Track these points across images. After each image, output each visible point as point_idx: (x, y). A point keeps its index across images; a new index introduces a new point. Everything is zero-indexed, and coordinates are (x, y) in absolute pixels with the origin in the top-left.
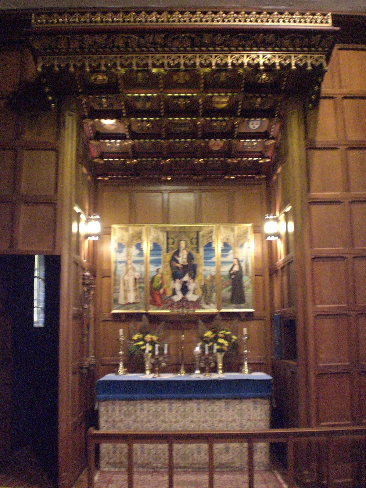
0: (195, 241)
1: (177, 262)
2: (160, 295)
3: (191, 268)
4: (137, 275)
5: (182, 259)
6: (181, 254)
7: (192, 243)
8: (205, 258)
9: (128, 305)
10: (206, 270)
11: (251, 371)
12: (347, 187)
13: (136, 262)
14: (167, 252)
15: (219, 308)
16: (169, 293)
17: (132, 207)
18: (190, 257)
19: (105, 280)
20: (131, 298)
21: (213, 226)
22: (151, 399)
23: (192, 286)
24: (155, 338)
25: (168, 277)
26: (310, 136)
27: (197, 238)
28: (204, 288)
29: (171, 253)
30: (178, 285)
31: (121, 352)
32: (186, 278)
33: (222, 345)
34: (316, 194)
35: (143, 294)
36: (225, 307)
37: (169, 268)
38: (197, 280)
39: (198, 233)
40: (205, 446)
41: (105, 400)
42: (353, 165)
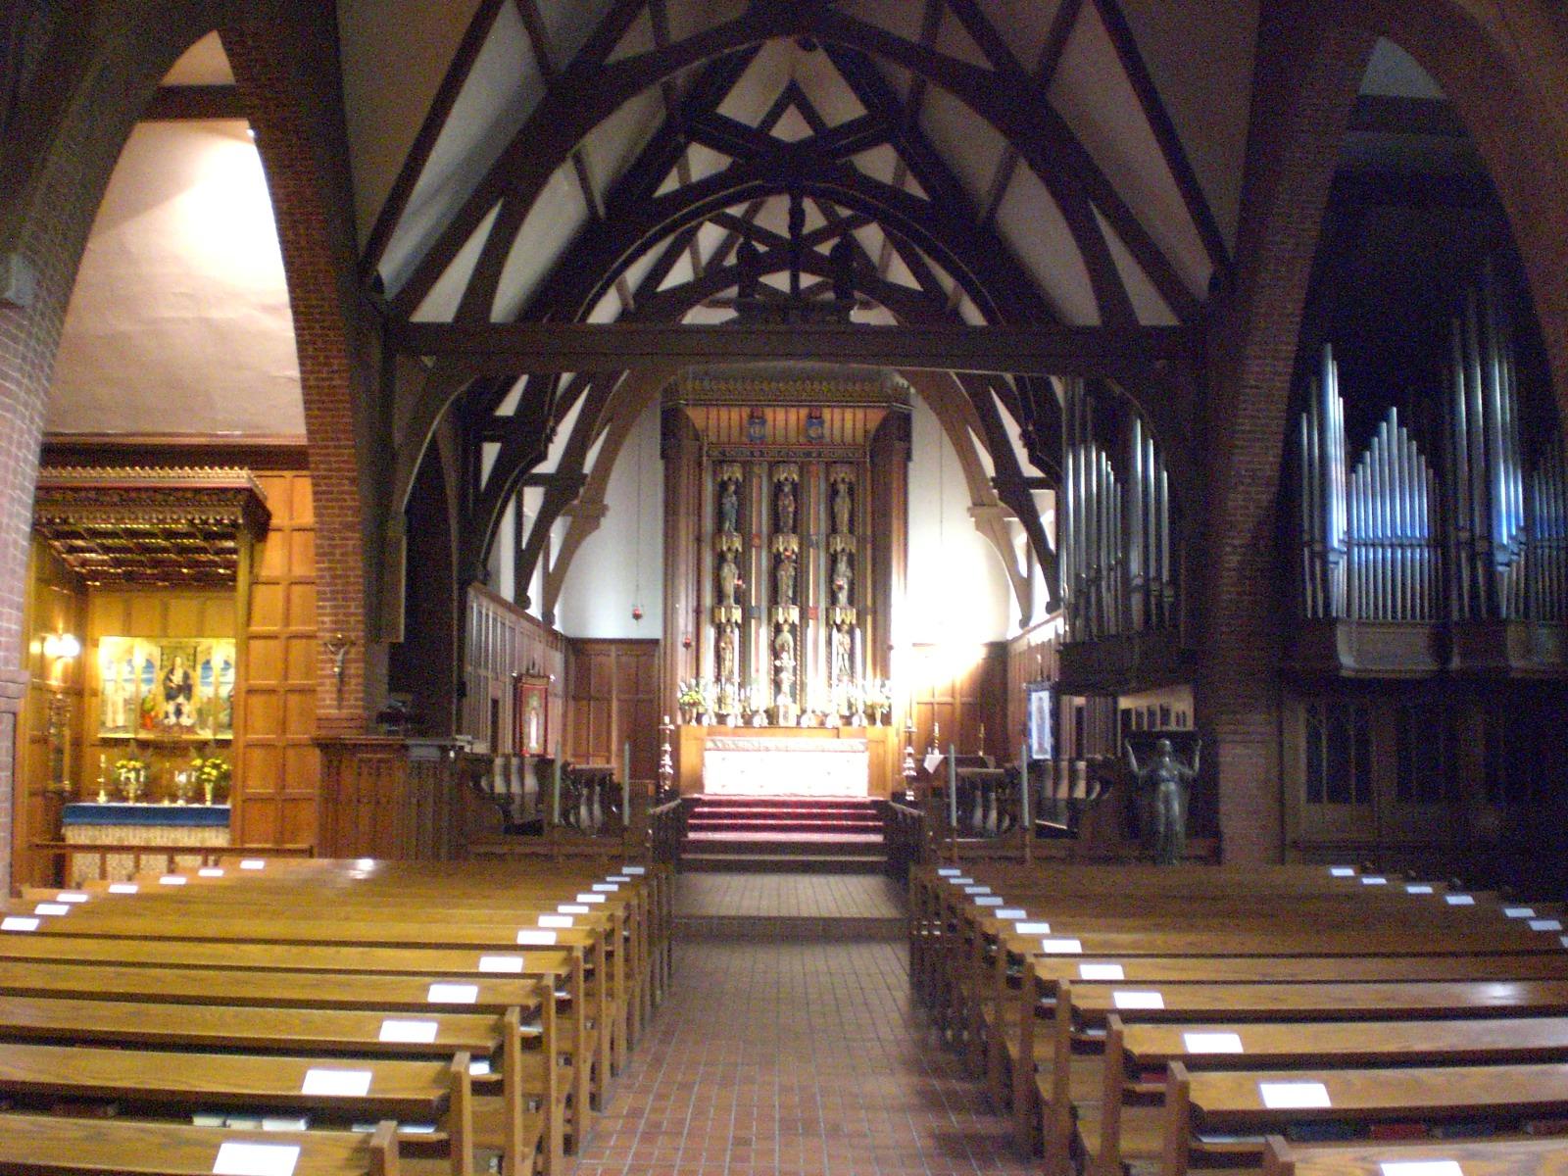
0: (191, 658)
1: (171, 681)
2: (151, 719)
3: (186, 689)
4: (127, 695)
5: (177, 678)
6: (175, 672)
7: (188, 660)
8: (203, 678)
9: (116, 729)
10: (203, 691)
11: (214, 802)
12: (287, 622)
13: (126, 680)
14: (161, 669)
15: (215, 734)
16: (161, 716)
17: (128, 614)
18: (186, 676)
19: (94, 699)
20: (121, 721)
21: (213, 642)
22: (115, 825)
23: (187, 708)
24: (138, 765)
25: (161, 698)
26: (255, 571)
27: (195, 655)
28: (200, 712)
29: (166, 670)
30: (171, 707)
31: (101, 780)
32: (181, 699)
33: (209, 774)
34: (254, 629)
35: (133, 716)
36: (222, 732)
37: (162, 688)
38: (192, 702)
39: (195, 648)
40: (97, 856)
41: (70, 824)
42: (296, 599)
